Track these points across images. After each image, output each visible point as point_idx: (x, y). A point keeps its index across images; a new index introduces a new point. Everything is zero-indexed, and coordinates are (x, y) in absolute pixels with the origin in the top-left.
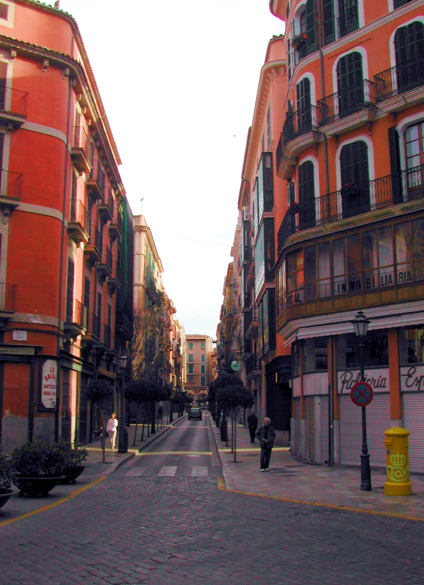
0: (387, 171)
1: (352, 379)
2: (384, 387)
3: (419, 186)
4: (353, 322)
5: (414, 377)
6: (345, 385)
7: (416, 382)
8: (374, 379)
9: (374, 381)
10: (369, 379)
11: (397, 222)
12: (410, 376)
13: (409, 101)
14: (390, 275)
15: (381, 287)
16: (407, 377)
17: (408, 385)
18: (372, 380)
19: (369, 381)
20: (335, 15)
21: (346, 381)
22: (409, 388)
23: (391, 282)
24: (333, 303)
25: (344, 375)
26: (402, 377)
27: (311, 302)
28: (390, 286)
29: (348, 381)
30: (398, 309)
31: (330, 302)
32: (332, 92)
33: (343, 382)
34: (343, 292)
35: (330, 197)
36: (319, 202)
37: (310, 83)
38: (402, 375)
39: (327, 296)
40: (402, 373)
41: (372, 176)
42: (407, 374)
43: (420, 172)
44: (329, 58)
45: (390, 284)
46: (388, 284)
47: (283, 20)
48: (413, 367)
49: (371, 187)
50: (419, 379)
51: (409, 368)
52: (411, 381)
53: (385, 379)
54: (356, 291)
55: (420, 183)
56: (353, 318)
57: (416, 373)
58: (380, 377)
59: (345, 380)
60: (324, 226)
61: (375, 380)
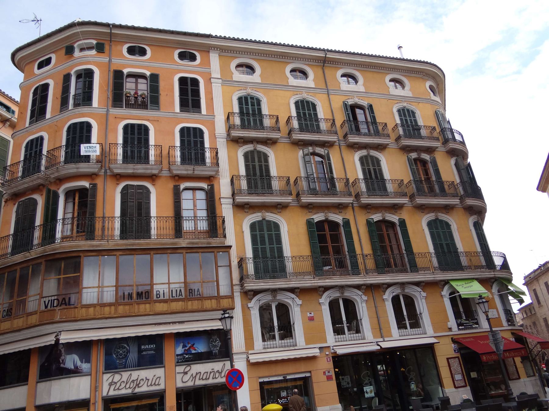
0: (170, 212)
1: (121, 381)
2: (159, 385)
3: (206, 230)
4: (220, 319)
5: (189, 374)
6: (113, 387)
7: (192, 378)
8: (147, 378)
9: (147, 381)
10: (123, 381)
11: (189, 251)
12: (186, 373)
13: (196, 172)
14: (176, 290)
15: (171, 298)
16: (183, 374)
17: (184, 381)
18: (145, 380)
19: (142, 380)
20: (71, 91)
21: (113, 383)
22: (184, 383)
23: (182, 295)
24: (116, 310)
25: (113, 376)
26: (177, 375)
27: (189, 300)
28: (177, 299)
29: (116, 383)
30: (189, 317)
31: (113, 308)
32: (61, 144)
33: (110, 385)
34: (128, 300)
35: (105, 220)
36: (61, 223)
37: (92, 127)
38: (178, 373)
39: (100, 303)
40: (177, 372)
41: (153, 212)
42: (183, 372)
43: (193, 221)
44: (115, 117)
45: (181, 297)
46: (178, 296)
47: (23, 71)
48: (189, 365)
49: (58, 224)
50: (194, 375)
51: (185, 366)
52: (186, 378)
53: (160, 377)
54: (144, 299)
55: (193, 229)
56: (220, 317)
57: (191, 370)
58: (154, 376)
59: (112, 382)
60: (108, 241)
61: (148, 380)
